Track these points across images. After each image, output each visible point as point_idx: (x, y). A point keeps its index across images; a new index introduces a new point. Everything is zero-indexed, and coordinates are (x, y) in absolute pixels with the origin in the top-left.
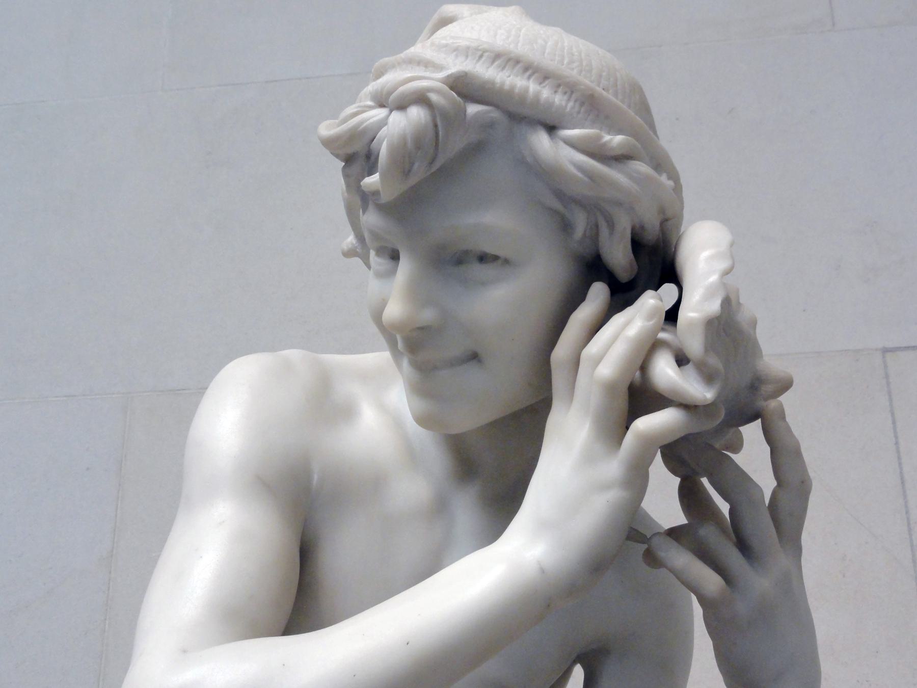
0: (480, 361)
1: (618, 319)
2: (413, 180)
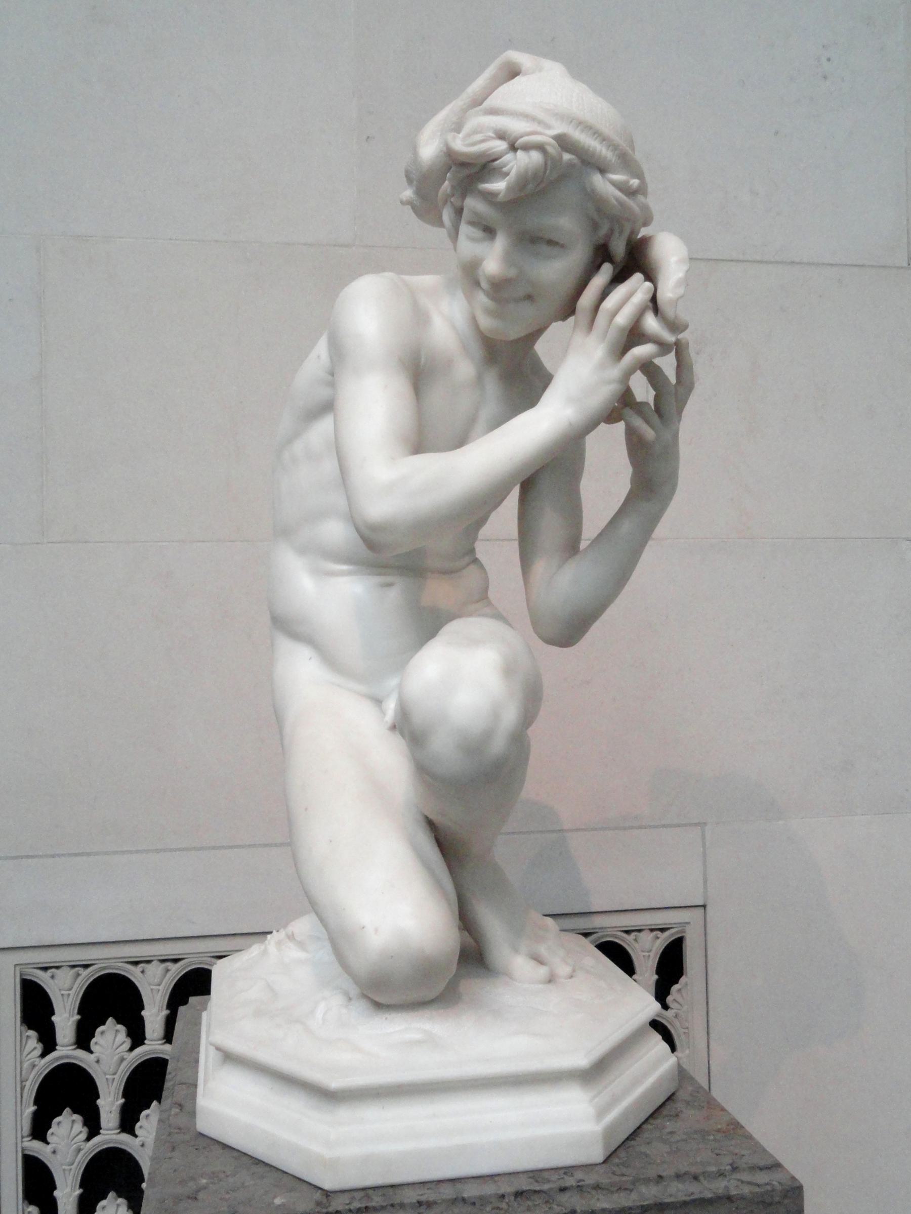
1: (621, 290)
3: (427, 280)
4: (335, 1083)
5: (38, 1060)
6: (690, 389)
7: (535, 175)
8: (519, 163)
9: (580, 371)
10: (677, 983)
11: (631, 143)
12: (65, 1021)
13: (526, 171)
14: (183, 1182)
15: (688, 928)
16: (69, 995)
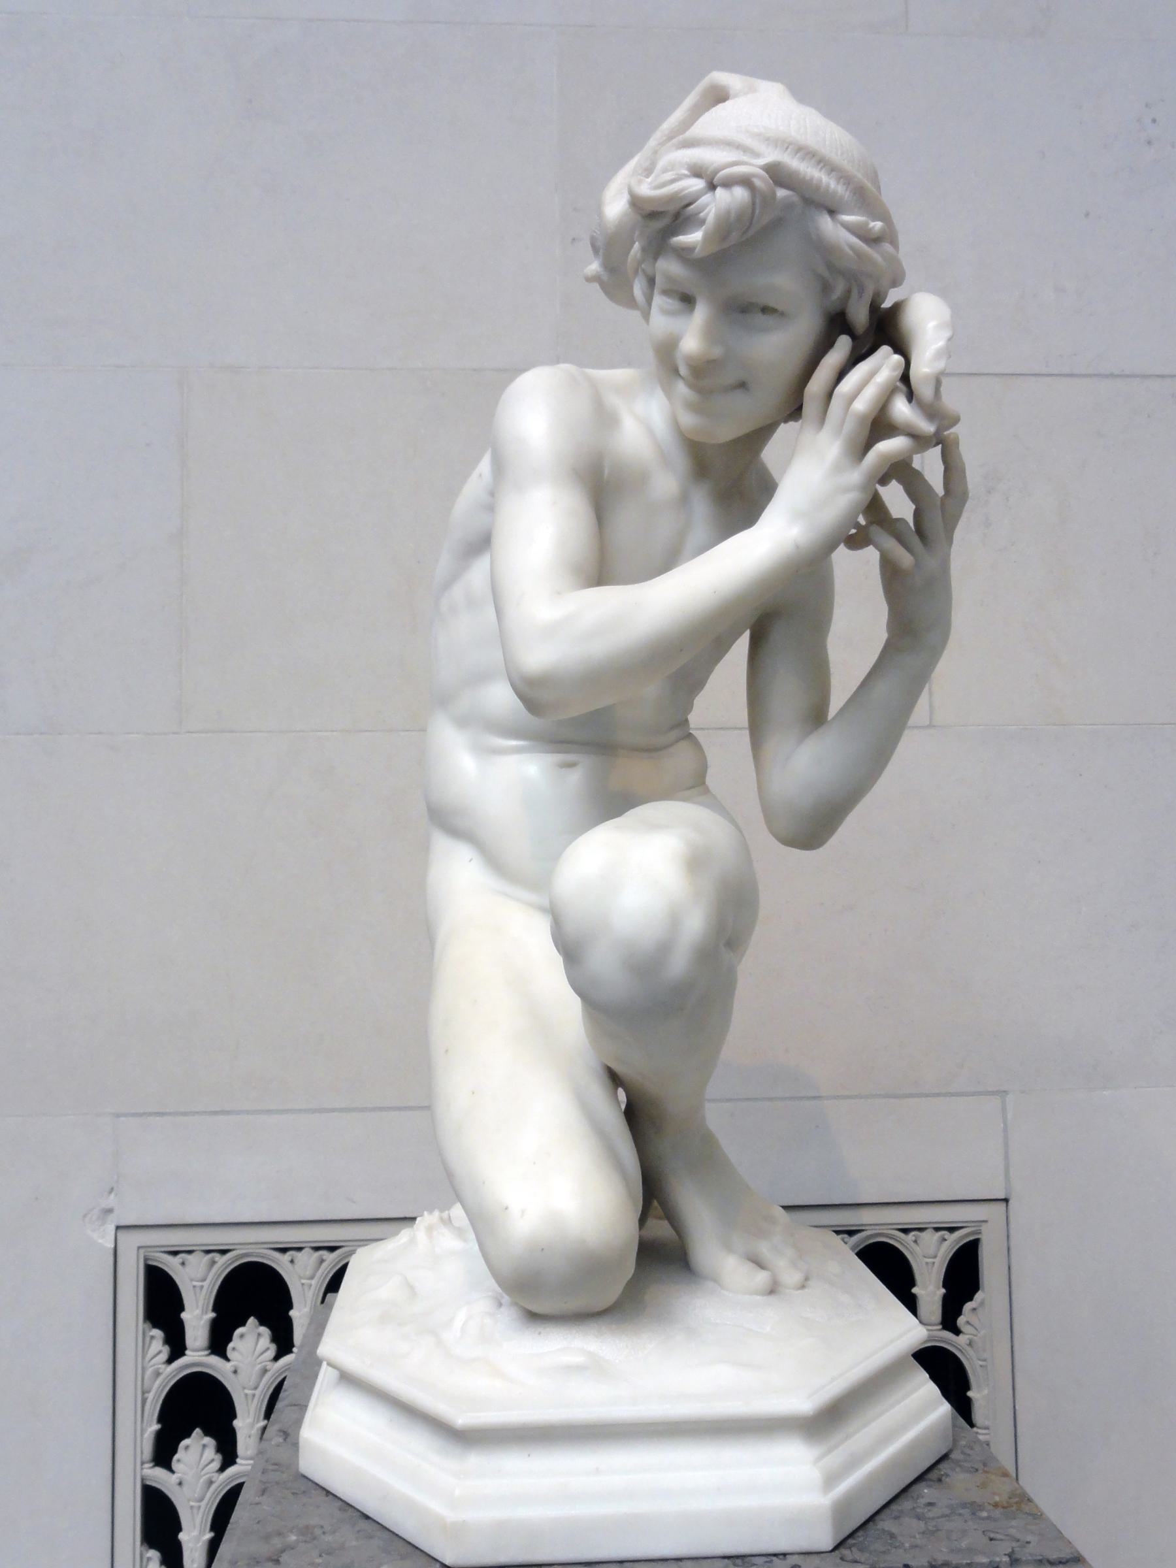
0: (747, 389)
2: (726, 245)
3: (620, 375)
4: (461, 1419)
5: (163, 1366)
6: (964, 497)
7: (740, 216)
8: (718, 204)
9: (811, 479)
10: (971, 1299)
11: (875, 179)
12: (197, 1319)
13: (728, 212)
14: (267, 1538)
15: (984, 1228)
16: (202, 1287)
